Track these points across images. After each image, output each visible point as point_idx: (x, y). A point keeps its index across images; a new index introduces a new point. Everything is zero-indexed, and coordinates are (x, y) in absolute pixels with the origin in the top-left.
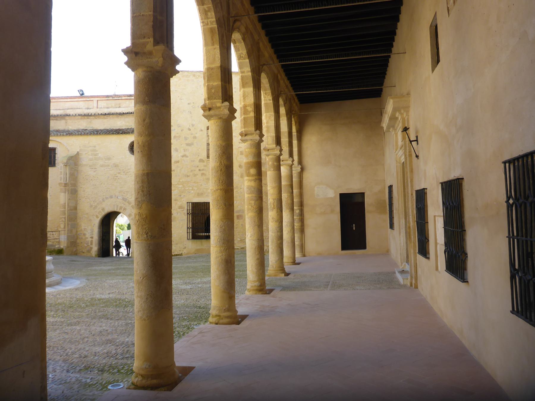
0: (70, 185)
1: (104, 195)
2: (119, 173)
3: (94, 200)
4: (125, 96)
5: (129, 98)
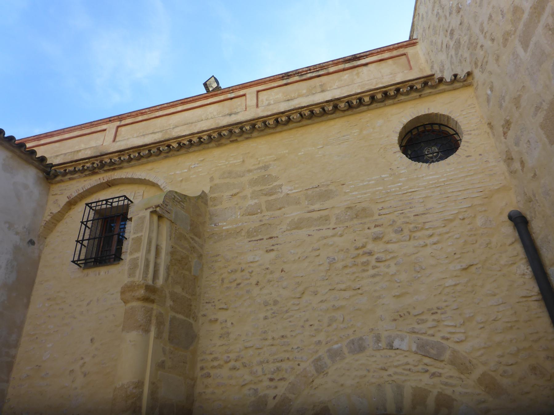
0: (169, 303)
1: (319, 342)
2: (376, 239)
3: (273, 373)
4: (336, 62)
5: (348, 65)
